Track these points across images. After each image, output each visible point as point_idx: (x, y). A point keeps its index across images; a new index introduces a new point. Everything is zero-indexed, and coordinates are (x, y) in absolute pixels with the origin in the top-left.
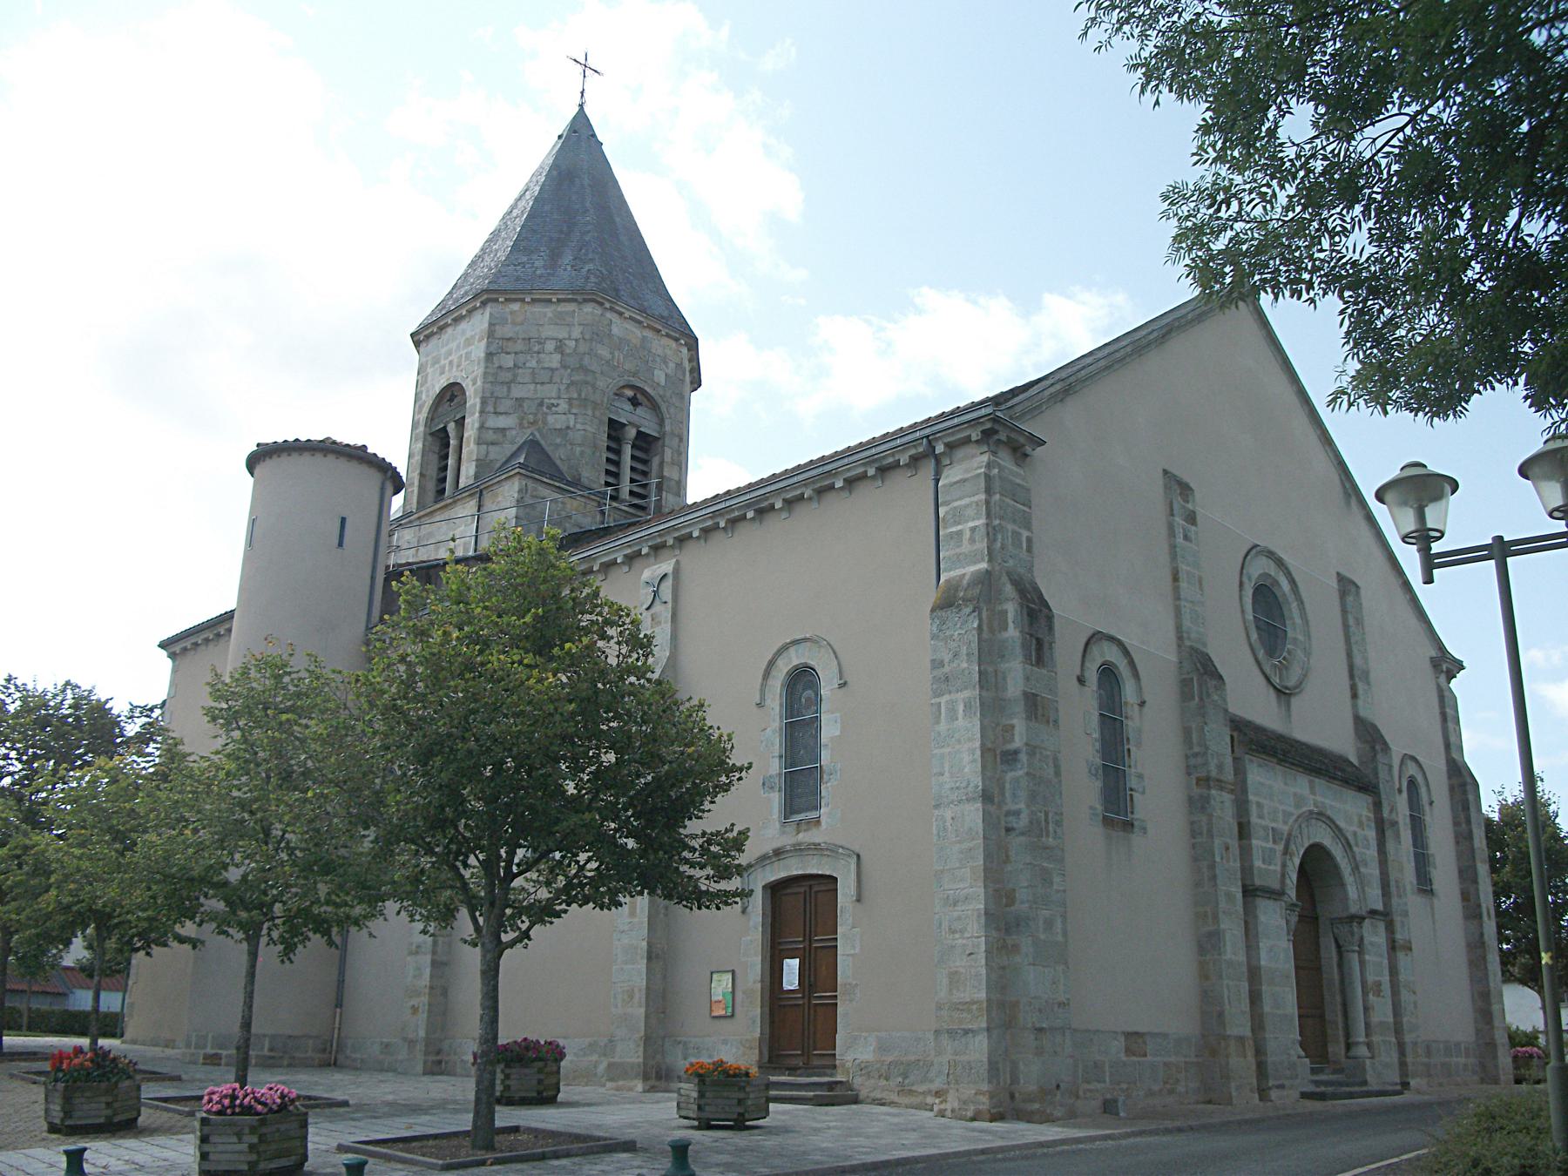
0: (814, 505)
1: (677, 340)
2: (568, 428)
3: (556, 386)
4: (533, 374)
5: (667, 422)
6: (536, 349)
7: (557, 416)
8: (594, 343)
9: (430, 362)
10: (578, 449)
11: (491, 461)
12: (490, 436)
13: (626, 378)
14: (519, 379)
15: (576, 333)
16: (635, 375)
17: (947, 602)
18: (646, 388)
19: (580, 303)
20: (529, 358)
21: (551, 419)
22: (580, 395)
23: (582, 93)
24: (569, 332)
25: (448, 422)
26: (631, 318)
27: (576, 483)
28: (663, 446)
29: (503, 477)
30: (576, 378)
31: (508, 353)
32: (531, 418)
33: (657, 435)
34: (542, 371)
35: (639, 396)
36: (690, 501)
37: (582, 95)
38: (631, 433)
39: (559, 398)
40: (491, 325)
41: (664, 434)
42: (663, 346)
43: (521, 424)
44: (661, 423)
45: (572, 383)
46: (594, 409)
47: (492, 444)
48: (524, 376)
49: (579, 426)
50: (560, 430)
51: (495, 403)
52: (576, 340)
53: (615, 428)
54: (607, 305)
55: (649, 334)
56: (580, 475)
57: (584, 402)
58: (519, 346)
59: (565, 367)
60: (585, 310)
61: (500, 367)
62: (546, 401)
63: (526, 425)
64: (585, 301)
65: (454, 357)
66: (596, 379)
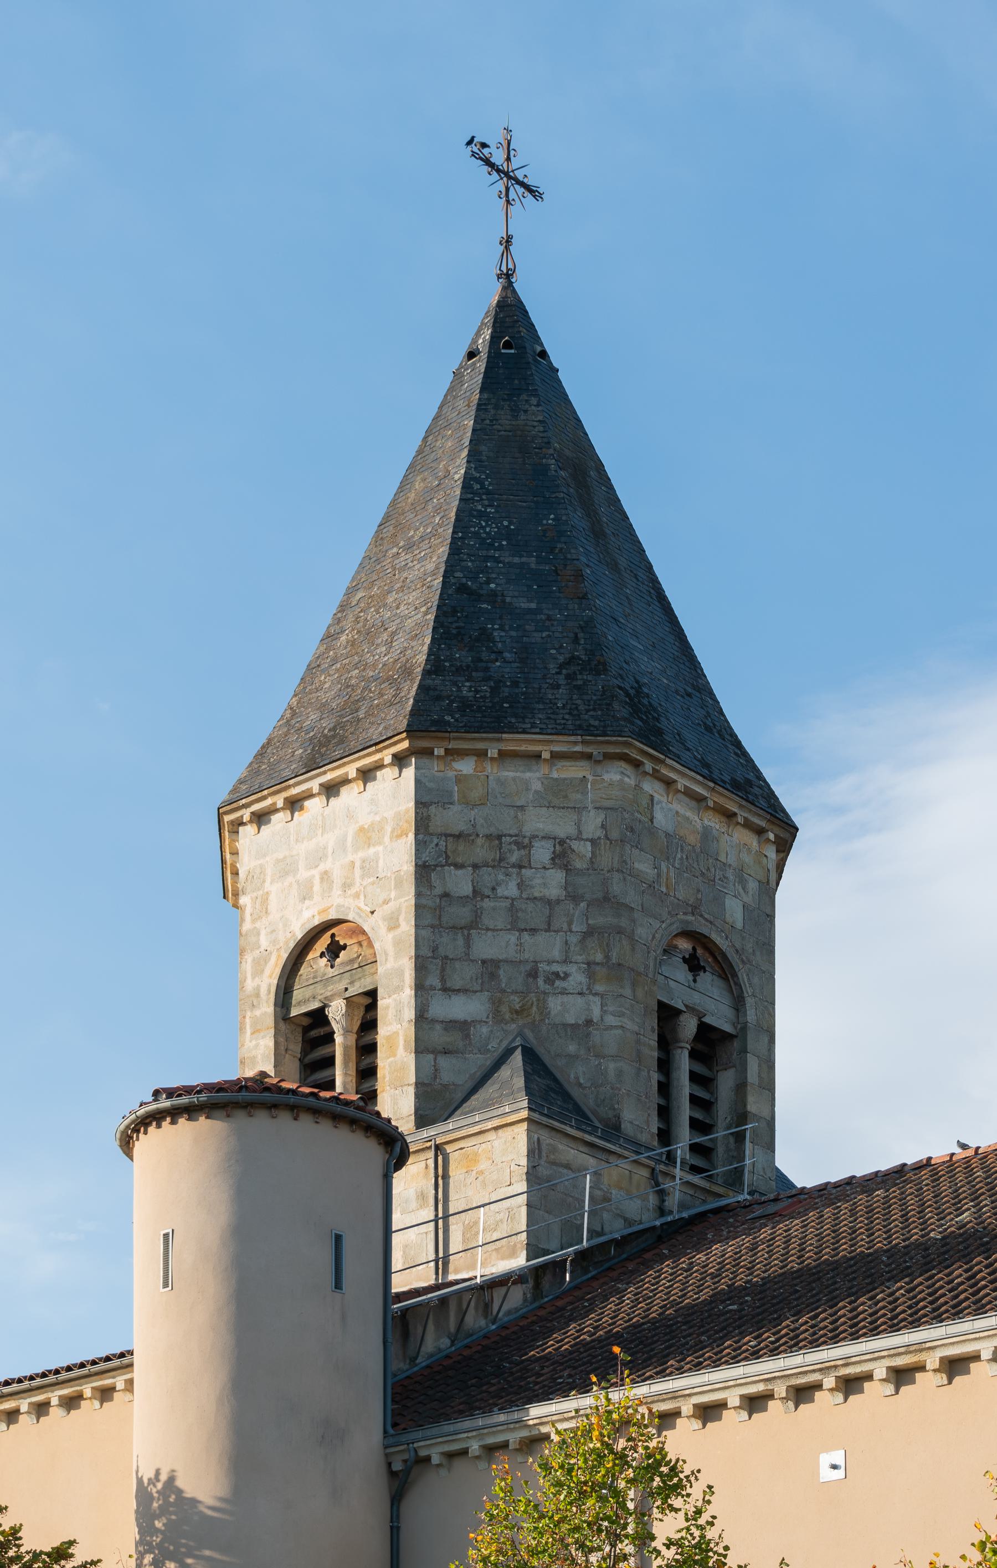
1: (760, 832)
2: (589, 1022)
3: (558, 939)
4: (512, 910)
5: (750, 1001)
6: (514, 858)
8: (628, 847)
9: (269, 872)
10: (612, 1066)
11: (445, 1087)
12: (438, 1037)
13: (681, 916)
14: (486, 921)
15: (592, 824)
16: (695, 909)
18: (714, 936)
20: (501, 877)
21: (554, 1004)
22: (607, 957)
23: (507, 242)
24: (578, 825)
25: (330, 999)
26: (688, 793)
27: (613, 1129)
28: (744, 1051)
29: (490, 1125)
30: (599, 920)
31: (458, 866)
32: (516, 1001)
33: (727, 1028)
34: (530, 907)
35: (700, 952)
37: (507, 248)
38: (688, 1027)
39: (566, 961)
40: (421, 804)
41: (744, 1029)
43: (497, 1015)
44: (738, 1003)
45: (589, 933)
46: (634, 985)
47: (446, 1052)
49: (610, 1020)
50: (575, 1027)
51: (443, 970)
52: (593, 842)
54: (648, 766)
55: (714, 822)
57: (616, 970)
58: (481, 851)
59: (575, 898)
60: (606, 777)
61: (446, 895)
62: (543, 967)
63: (507, 1016)
64: (608, 757)
65: (334, 866)
66: (634, 921)
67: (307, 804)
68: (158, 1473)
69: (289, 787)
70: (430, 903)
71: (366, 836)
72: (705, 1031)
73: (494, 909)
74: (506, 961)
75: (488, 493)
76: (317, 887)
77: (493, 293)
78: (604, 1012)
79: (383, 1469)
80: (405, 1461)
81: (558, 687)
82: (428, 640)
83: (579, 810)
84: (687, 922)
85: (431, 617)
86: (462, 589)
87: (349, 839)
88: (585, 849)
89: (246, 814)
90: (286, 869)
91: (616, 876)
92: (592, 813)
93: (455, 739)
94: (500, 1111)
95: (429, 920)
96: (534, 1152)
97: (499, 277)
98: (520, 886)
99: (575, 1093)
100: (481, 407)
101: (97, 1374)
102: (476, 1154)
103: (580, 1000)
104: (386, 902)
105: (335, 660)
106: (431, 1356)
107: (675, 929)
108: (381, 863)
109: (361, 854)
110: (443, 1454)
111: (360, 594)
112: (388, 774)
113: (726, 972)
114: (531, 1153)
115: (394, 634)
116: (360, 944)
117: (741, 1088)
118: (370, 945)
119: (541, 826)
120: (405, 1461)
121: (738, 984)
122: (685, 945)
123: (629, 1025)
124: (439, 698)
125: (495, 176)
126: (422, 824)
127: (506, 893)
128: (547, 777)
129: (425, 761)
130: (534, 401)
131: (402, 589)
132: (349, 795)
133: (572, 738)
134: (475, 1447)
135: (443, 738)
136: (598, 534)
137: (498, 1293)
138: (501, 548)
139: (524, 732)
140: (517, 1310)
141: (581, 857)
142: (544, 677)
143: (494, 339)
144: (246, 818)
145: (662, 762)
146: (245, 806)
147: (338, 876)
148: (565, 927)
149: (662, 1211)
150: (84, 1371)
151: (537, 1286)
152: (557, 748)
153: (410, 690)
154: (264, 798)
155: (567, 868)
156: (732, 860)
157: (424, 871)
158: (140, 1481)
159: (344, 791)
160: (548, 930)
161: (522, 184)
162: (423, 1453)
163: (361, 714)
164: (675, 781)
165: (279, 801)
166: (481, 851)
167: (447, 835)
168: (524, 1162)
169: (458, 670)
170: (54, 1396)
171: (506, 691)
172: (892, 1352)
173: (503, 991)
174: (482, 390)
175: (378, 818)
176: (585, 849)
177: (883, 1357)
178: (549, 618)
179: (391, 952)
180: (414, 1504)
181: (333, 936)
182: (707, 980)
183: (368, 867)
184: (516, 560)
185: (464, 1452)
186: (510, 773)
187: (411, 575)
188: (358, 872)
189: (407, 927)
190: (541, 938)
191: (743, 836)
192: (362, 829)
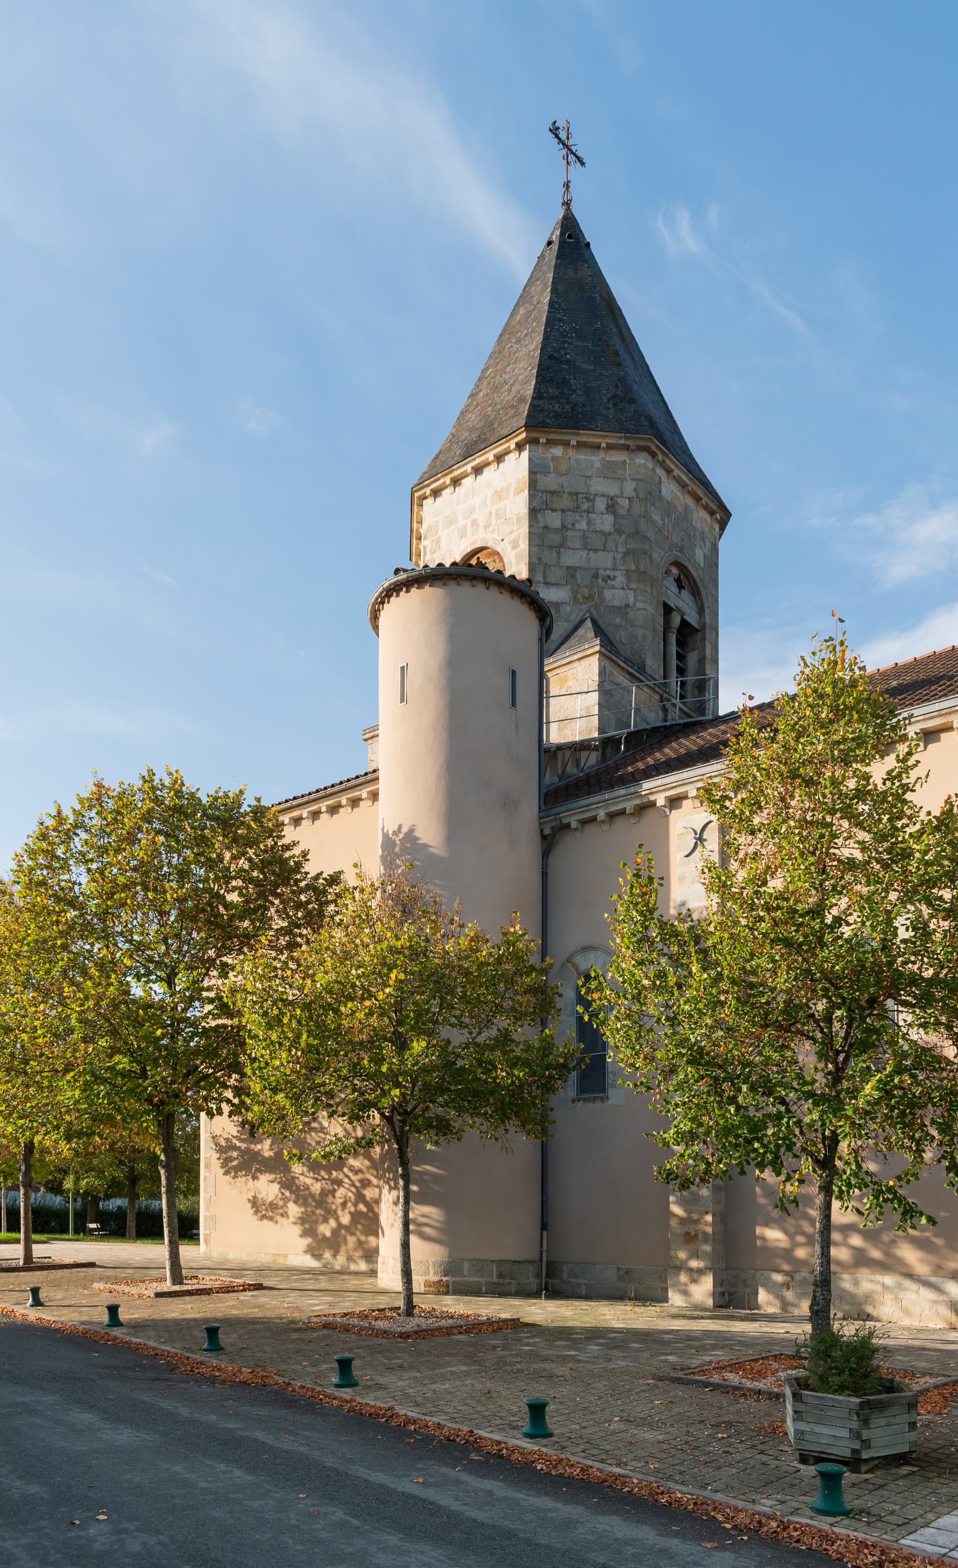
0: (605, 827)
2: (627, 606)
3: (610, 555)
4: (584, 537)
5: (707, 611)
6: (585, 507)
7: (614, 591)
10: (640, 632)
14: (569, 543)
15: (629, 488)
17: (554, 1122)
18: (690, 568)
19: (633, 451)
20: (577, 518)
21: (608, 594)
22: (637, 567)
23: (567, 185)
24: (621, 488)
27: (642, 668)
28: (704, 639)
29: (575, 657)
30: (633, 545)
31: (553, 510)
32: (586, 592)
33: (695, 625)
34: (594, 536)
35: (682, 577)
36: (722, 712)
38: (676, 621)
39: (614, 569)
40: (532, 473)
41: (704, 626)
42: (700, 518)
43: (575, 599)
44: (701, 611)
45: (627, 553)
46: (652, 585)
48: (574, 540)
49: (639, 605)
50: (619, 608)
51: (545, 571)
52: (630, 499)
53: (668, 610)
54: (660, 457)
55: (690, 502)
56: (644, 662)
57: (643, 576)
58: (566, 502)
59: (619, 531)
60: (637, 461)
62: (601, 572)
63: (581, 600)
64: (640, 449)
65: (481, 517)
67: (463, 481)
68: (400, 827)
69: (453, 471)
70: (537, 532)
71: (499, 495)
72: (684, 623)
73: (573, 537)
74: (580, 568)
75: (563, 309)
76: (469, 530)
77: (560, 214)
78: (636, 600)
79: (539, 832)
80: (552, 828)
81: (609, 409)
82: (534, 382)
83: (622, 480)
84: (678, 557)
85: (535, 371)
86: (551, 357)
87: (489, 498)
88: (625, 503)
89: (428, 491)
90: (451, 521)
91: (643, 520)
92: (629, 482)
93: (552, 432)
94: (583, 648)
95: (536, 542)
96: (602, 673)
97: (563, 204)
98: (588, 523)
99: (619, 647)
100: (556, 267)
101: (350, 788)
102: (566, 677)
103: (622, 593)
104: (511, 533)
105: (477, 406)
106: (548, 786)
107: (672, 559)
108: (508, 511)
109: (496, 507)
110: (578, 821)
111: (490, 371)
112: (513, 456)
113: (696, 592)
114: (600, 673)
115: (512, 385)
116: (494, 561)
117: (702, 661)
118: (501, 559)
119: (600, 488)
120: (552, 828)
121: (701, 600)
122: (675, 571)
123: (650, 609)
124: (542, 411)
125: (561, 146)
126: (533, 485)
127: (580, 528)
128: (603, 459)
129: (535, 447)
130: (586, 265)
131: (515, 362)
132: (488, 472)
133: (619, 435)
134: (601, 814)
135: (545, 432)
136: (623, 339)
137: (584, 754)
138: (572, 337)
139: (592, 430)
140: (594, 766)
141: (623, 508)
142: (601, 403)
143: (562, 234)
144: (428, 493)
145: (667, 455)
146: (427, 486)
147: (482, 522)
148: (614, 548)
149: (665, 720)
150: (343, 786)
151: (604, 754)
152: (611, 441)
153: (525, 409)
154: (439, 479)
155: (615, 514)
156: (698, 526)
157: (533, 512)
158: (385, 836)
159: (486, 471)
160: (604, 550)
161: (575, 155)
162: (565, 821)
163: (495, 426)
164: (672, 470)
165: (447, 480)
166: (566, 502)
167: (547, 492)
168: (596, 678)
169: (552, 398)
170: (323, 806)
171: (580, 410)
172: (927, 716)
173: (578, 585)
174: (557, 258)
175: (506, 484)
176: (625, 503)
177: (919, 721)
178: (601, 374)
179: (514, 562)
180: (559, 857)
181: (478, 558)
182: (685, 593)
183: (500, 514)
184: (581, 344)
185: (594, 819)
186: (583, 456)
187: (520, 355)
188: (494, 517)
189: (524, 546)
190: (600, 555)
191: (703, 514)
192: (496, 492)
